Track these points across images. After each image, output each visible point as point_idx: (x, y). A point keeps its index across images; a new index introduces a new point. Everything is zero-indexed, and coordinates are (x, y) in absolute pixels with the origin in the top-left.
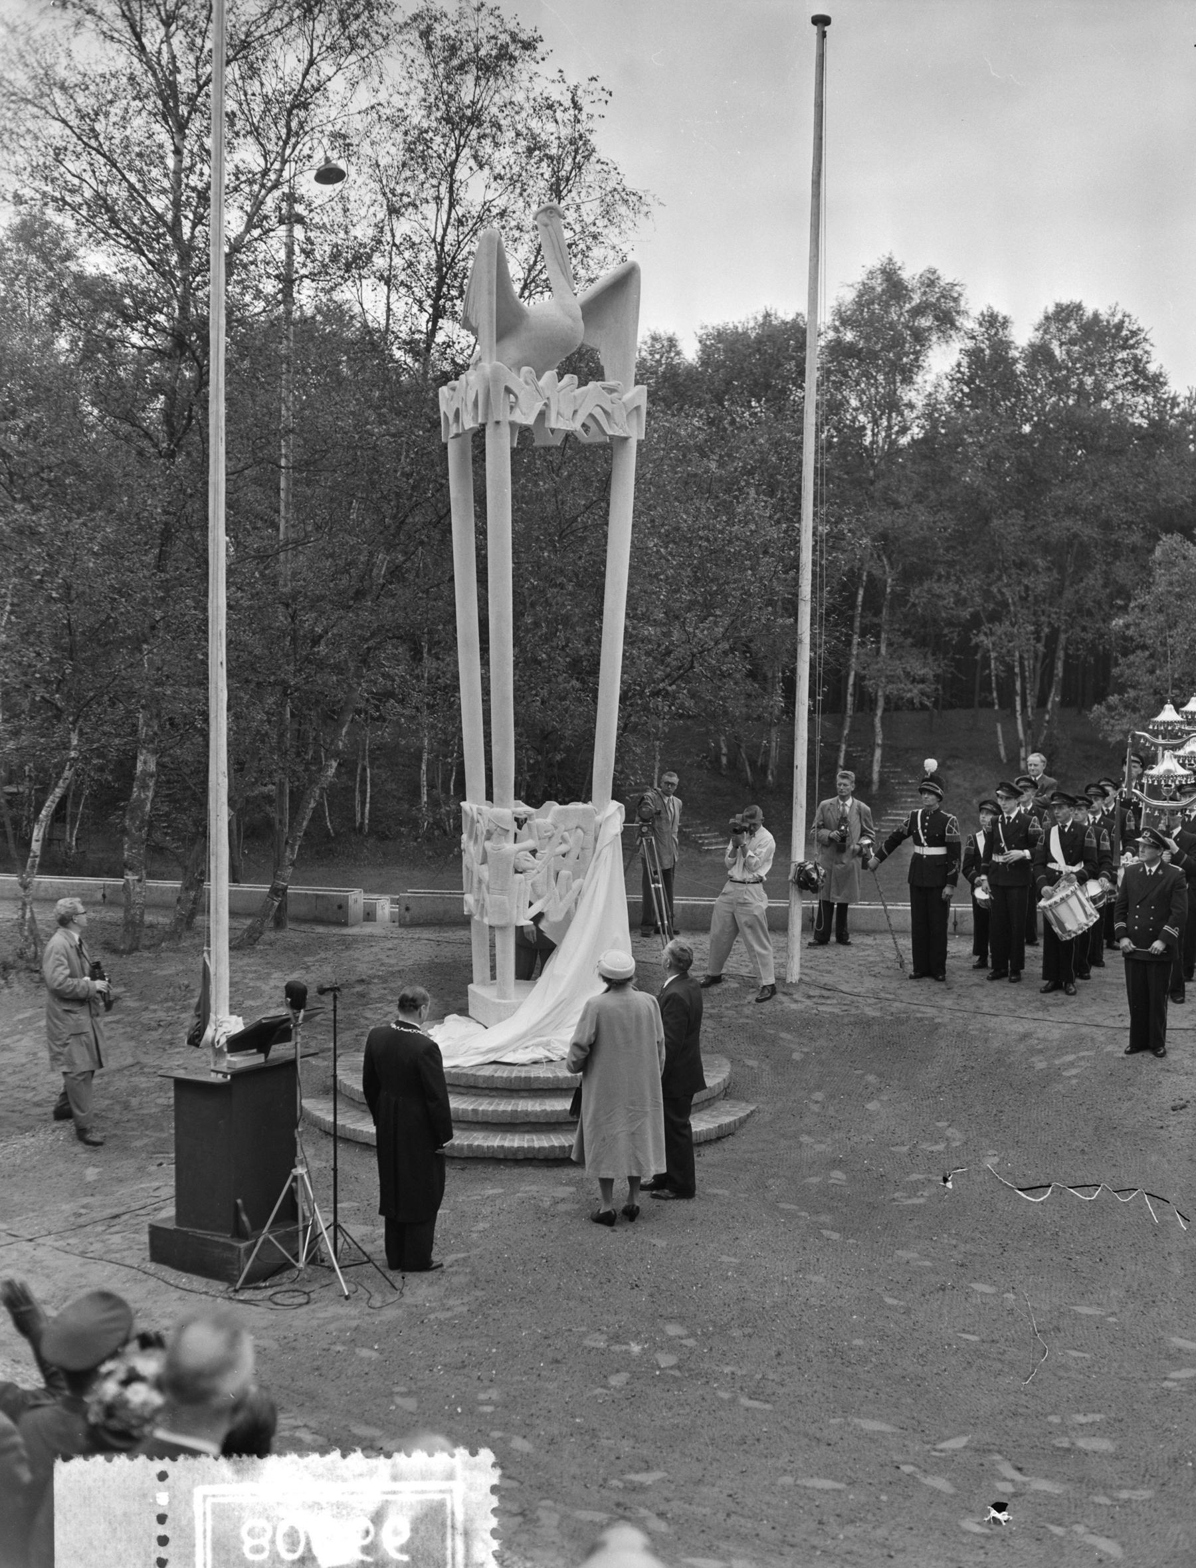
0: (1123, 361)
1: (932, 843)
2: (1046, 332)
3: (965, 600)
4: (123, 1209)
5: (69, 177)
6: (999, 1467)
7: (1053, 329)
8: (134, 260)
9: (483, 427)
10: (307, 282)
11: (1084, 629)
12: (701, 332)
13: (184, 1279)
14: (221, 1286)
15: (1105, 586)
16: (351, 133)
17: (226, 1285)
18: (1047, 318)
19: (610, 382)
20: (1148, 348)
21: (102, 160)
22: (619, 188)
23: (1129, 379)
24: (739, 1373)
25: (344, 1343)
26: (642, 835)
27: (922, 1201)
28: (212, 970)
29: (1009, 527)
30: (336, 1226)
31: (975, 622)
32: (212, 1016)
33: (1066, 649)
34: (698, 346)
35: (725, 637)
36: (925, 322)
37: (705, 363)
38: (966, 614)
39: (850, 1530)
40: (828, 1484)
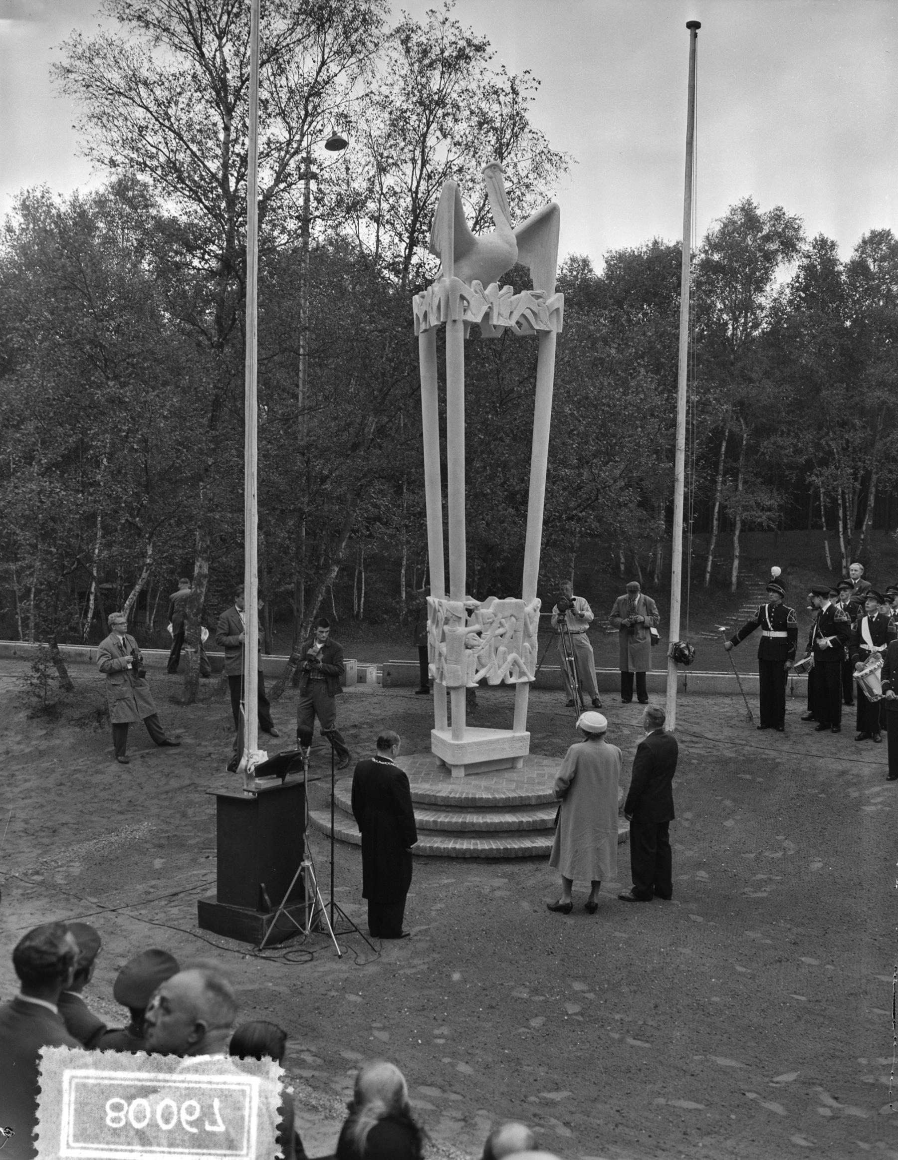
2: (862, 253)
4: (180, 889)
5: (149, 148)
6: (821, 1096)
8: (195, 206)
11: (890, 471)
12: (606, 255)
13: (223, 941)
14: (250, 947)
17: (253, 945)
18: (864, 242)
21: (172, 135)
22: (546, 151)
24: (627, 1019)
25: (337, 991)
27: (765, 894)
29: (834, 396)
31: (809, 466)
33: (876, 486)
34: (605, 265)
36: (773, 246)
38: (802, 460)
40: (692, 1105)
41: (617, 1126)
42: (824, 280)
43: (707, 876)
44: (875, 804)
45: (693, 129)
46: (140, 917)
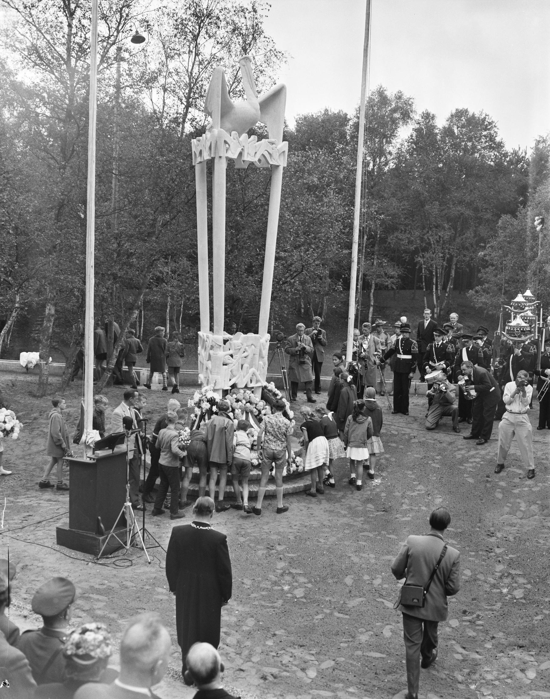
0: (484, 136)
1: (405, 353)
2: (451, 122)
3: (412, 241)
4: (43, 519)
5: (19, 35)
6: (455, 647)
7: (454, 120)
8: (48, 75)
9: (213, 160)
10: (128, 88)
11: (465, 256)
12: (297, 117)
13: (73, 553)
14: (91, 557)
15: (474, 237)
16: (151, 19)
17: (93, 556)
18: (452, 116)
19: (271, 140)
20: (496, 130)
21: (35, 29)
22: (273, 49)
23: (487, 144)
24: (333, 600)
25: (150, 585)
26: (278, 347)
27: (409, 519)
28: (85, 409)
29: (433, 209)
30: (144, 529)
31: (416, 252)
32: (85, 430)
33: (456, 265)
34: (296, 123)
35: (318, 259)
36: (397, 115)
37: (297, 131)
38: (412, 248)
39: (390, 677)
40: (378, 655)
41: (334, 670)
42: (428, 138)
43: (373, 507)
44: (472, 463)
45: (368, 41)
46: (18, 538)
